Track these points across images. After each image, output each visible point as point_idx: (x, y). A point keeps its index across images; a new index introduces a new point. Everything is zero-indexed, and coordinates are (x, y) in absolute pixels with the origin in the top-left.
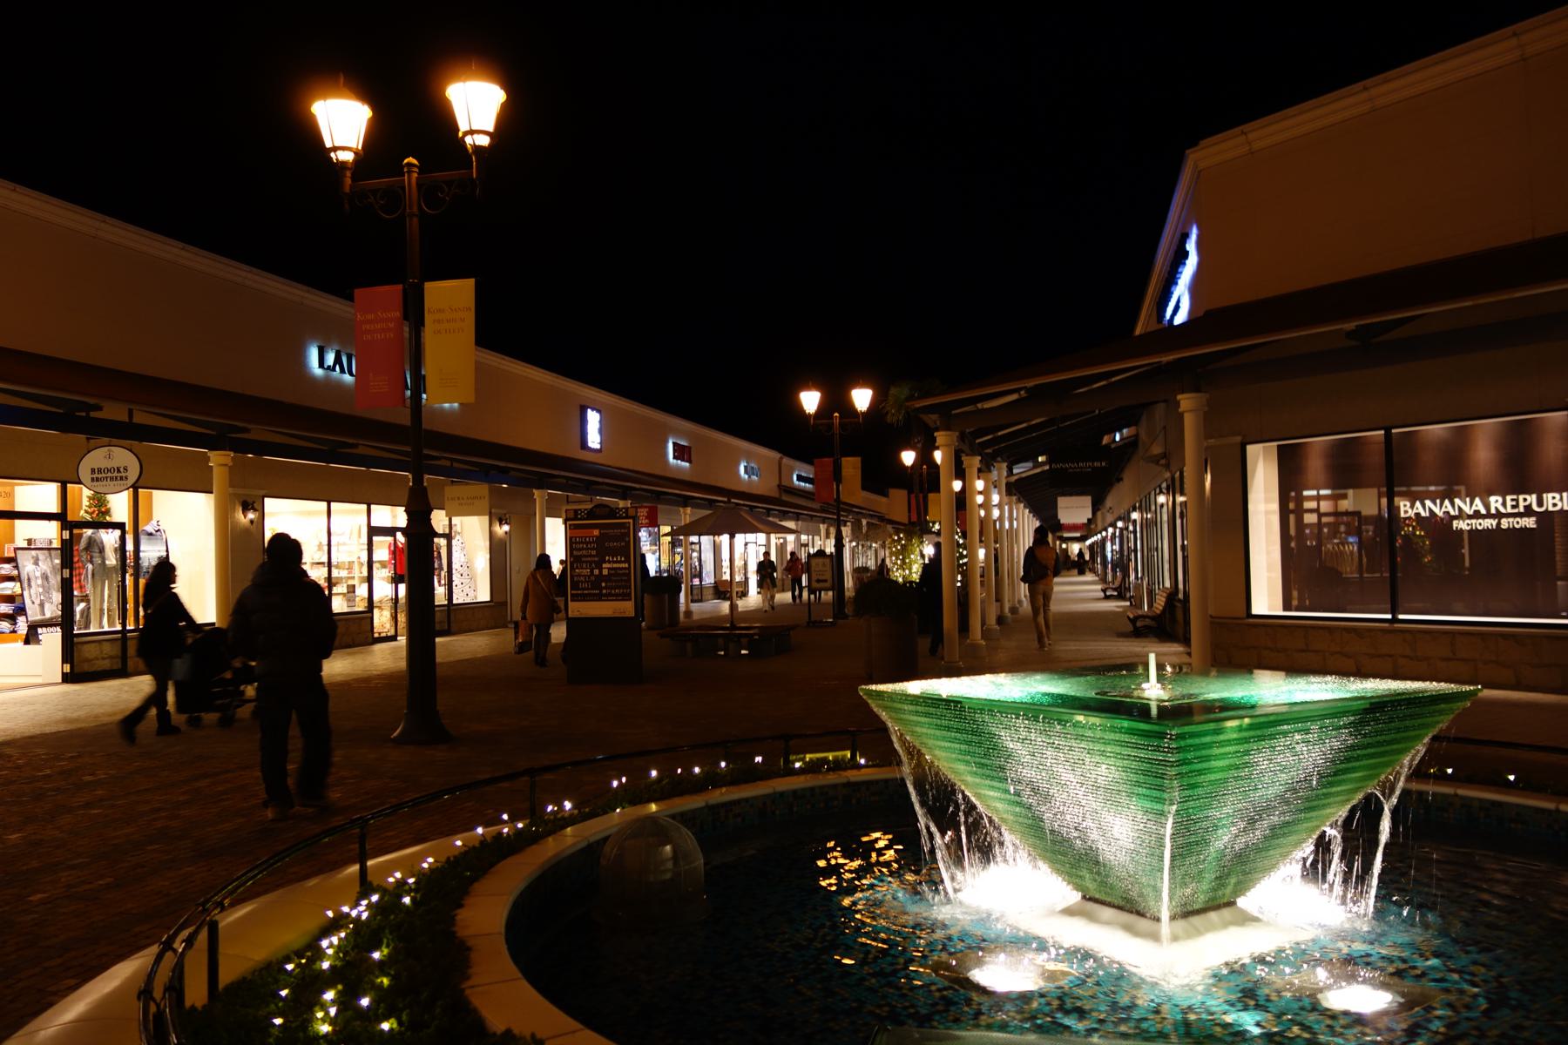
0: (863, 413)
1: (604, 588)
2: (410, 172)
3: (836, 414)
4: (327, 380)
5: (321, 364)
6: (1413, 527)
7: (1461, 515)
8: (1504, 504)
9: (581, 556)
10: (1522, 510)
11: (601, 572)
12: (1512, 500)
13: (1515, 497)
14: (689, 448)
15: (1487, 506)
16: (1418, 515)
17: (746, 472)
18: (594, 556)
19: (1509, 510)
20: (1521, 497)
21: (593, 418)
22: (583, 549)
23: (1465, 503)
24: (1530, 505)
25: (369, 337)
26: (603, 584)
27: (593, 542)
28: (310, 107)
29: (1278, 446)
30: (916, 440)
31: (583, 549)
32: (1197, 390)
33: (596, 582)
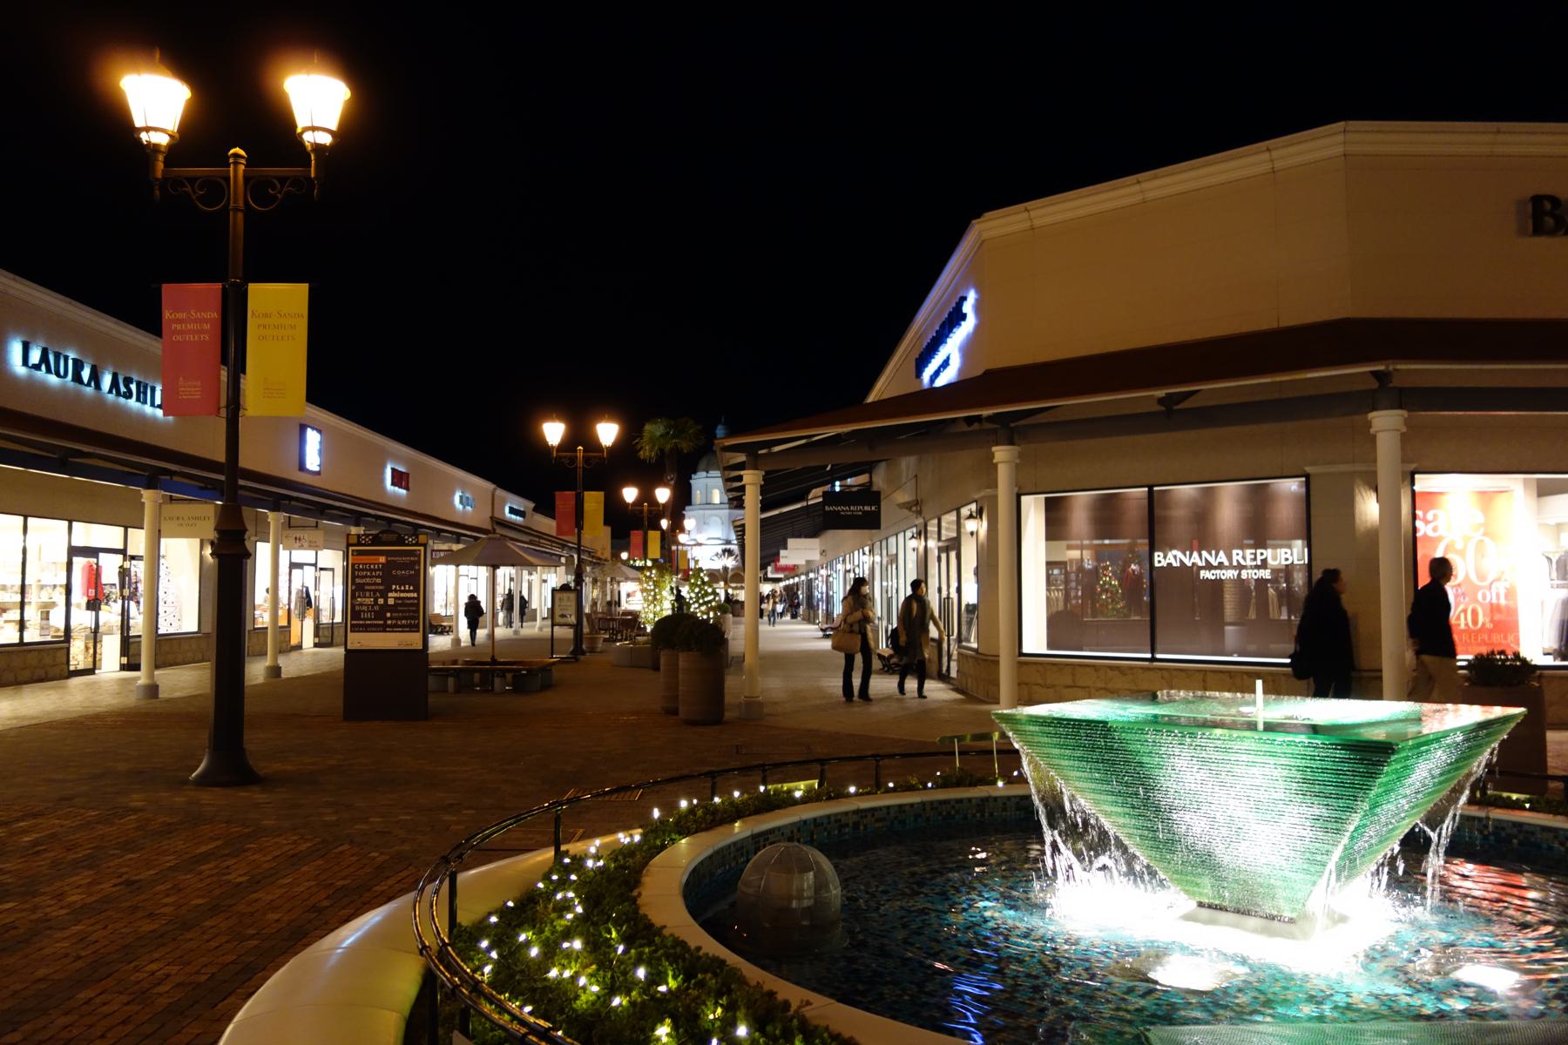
0: (607, 448)
1: (390, 619)
2: (236, 163)
3: (580, 448)
4: (30, 379)
5: (25, 361)
6: (1110, 578)
7: (1209, 566)
8: (1244, 558)
9: (364, 584)
10: (1259, 563)
11: (386, 601)
12: (1252, 554)
13: (1253, 551)
14: (408, 474)
15: (1230, 558)
16: (1170, 564)
17: (461, 502)
18: (378, 584)
19: (1249, 563)
20: (1259, 551)
21: (313, 438)
22: (366, 576)
23: (1211, 555)
24: (1266, 559)
25: (179, 338)
26: (388, 615)
27: (378, 570)
28: (119, 82)
29: (1046, 499)
30: (669, 478)
31: (366, 576)
32: (1011, 443)
33: (380, 613)
